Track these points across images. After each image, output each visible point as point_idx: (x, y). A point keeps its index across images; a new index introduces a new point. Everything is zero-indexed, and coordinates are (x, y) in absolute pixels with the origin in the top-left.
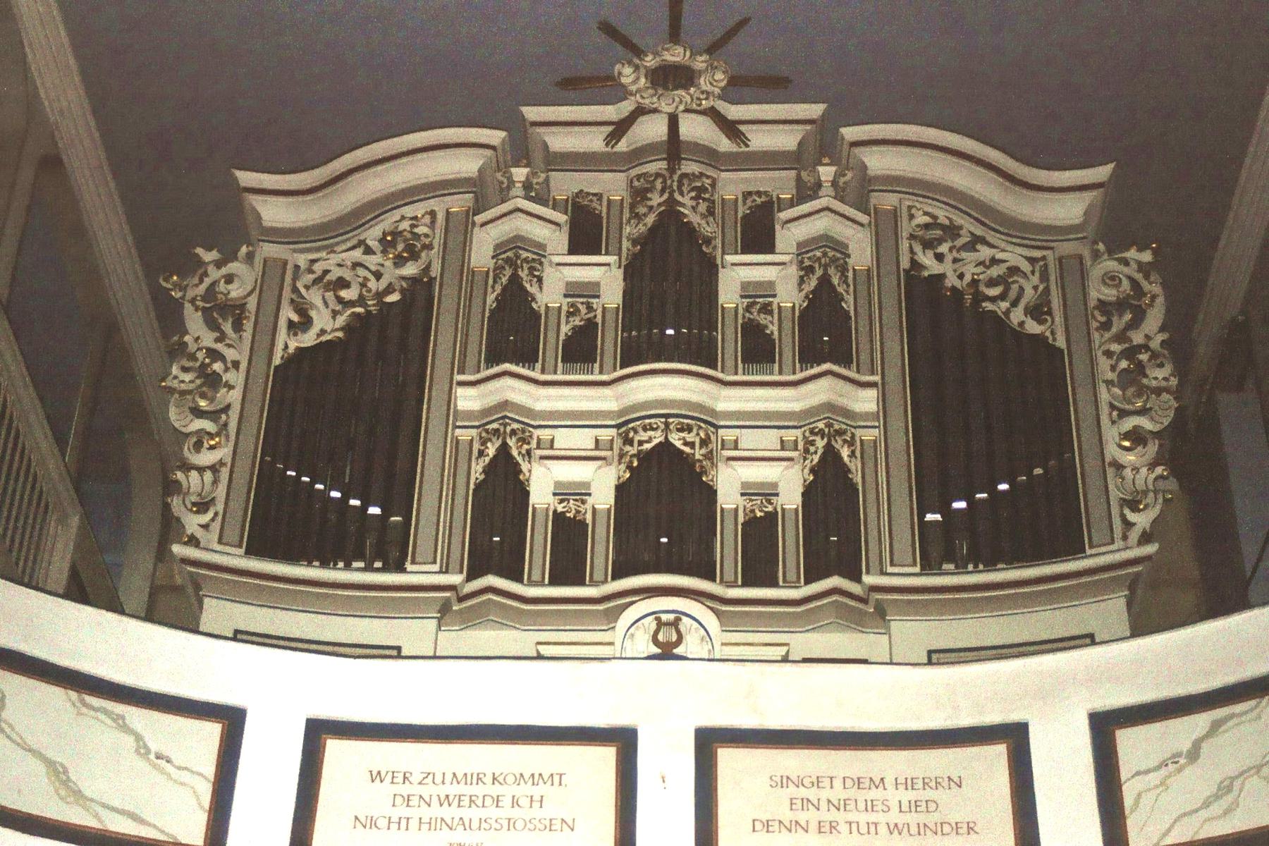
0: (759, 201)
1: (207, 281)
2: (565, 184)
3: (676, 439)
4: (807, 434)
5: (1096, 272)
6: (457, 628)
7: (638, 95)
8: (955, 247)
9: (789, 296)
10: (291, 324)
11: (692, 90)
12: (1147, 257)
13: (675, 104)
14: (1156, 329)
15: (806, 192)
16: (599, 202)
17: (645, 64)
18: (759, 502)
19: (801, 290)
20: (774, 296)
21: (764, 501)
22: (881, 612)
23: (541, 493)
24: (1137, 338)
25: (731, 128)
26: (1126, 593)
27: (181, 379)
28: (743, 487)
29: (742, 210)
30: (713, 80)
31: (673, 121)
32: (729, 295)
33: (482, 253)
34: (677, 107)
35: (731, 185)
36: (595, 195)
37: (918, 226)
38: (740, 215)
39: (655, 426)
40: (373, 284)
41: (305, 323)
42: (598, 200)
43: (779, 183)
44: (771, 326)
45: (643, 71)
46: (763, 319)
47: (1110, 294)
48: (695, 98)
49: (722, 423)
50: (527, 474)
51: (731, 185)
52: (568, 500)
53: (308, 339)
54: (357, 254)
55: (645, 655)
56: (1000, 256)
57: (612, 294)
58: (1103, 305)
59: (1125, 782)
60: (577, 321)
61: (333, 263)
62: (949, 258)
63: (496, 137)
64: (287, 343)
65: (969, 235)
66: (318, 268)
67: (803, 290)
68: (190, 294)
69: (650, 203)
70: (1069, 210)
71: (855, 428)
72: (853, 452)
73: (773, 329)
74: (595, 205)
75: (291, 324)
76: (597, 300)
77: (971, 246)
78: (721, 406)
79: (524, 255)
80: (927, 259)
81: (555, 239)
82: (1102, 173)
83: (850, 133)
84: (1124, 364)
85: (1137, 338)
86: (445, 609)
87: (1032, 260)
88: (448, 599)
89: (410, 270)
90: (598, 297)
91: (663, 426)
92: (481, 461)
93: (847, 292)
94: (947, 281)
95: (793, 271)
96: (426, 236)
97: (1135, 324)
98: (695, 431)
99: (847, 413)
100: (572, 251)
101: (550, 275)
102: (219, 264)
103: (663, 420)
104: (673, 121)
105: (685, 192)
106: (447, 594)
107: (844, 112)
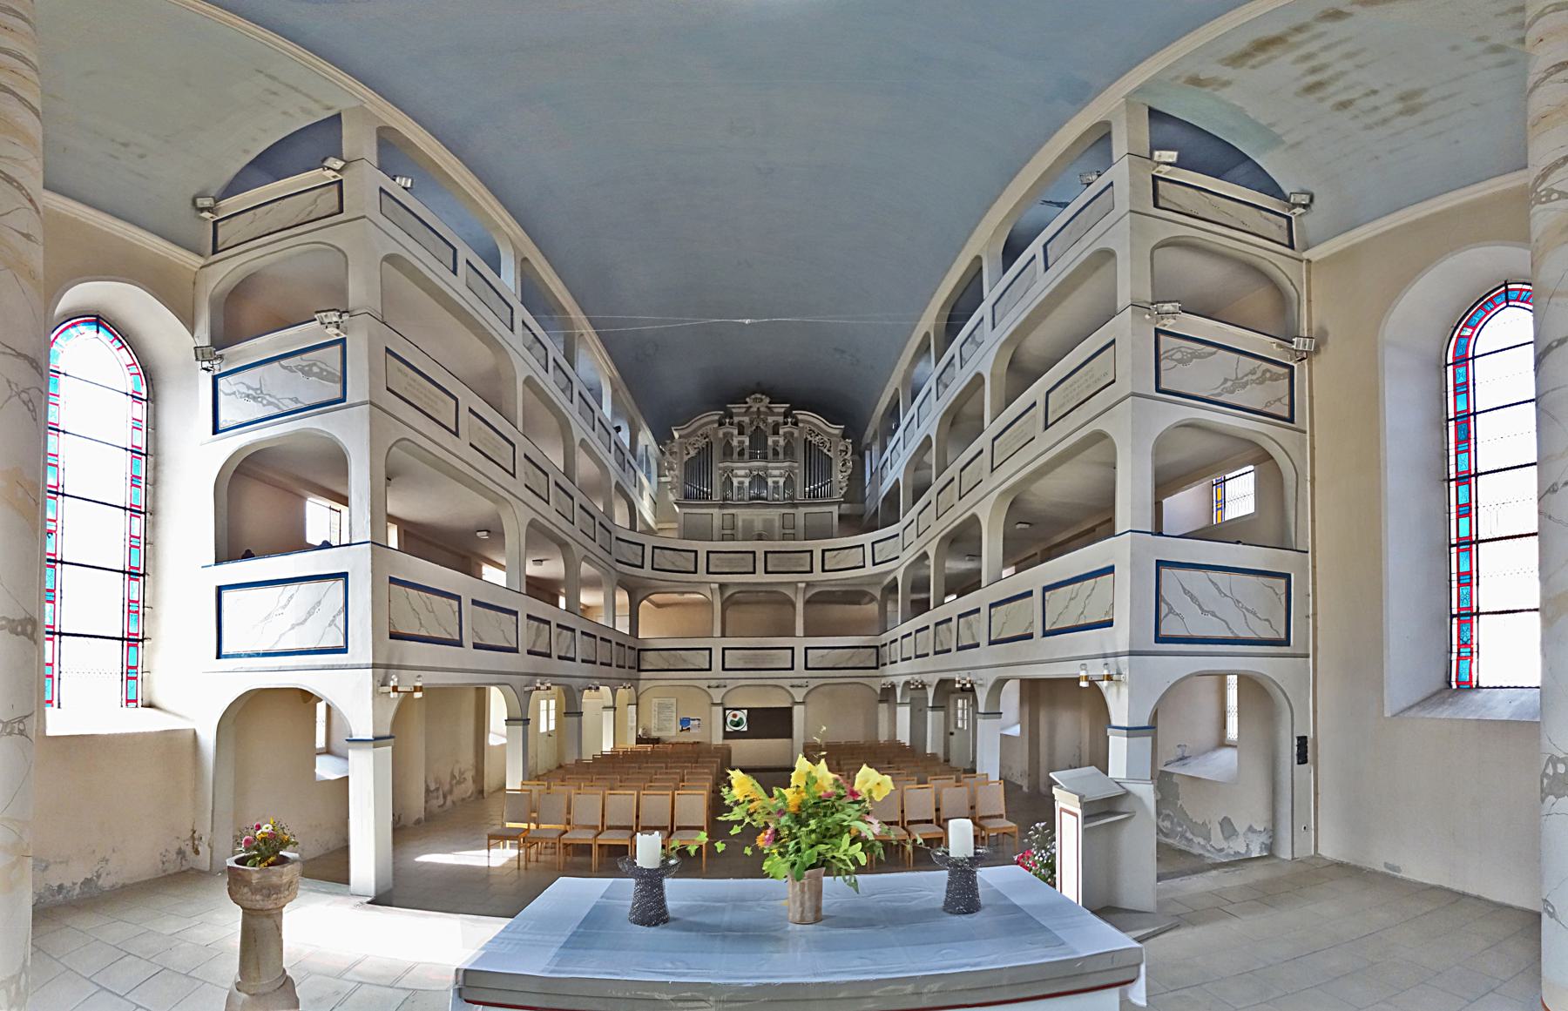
2: (736, 419)
9: (782, 442)
12: (850, 441)
14: (288, 868)
15: (786, 423)
23: (735, 481)
24: (846, 457)
25: (769, 408)
32: (770, 442)
33: (721, 435)
35: (770, 419)
41: (688, 454)
43: (781, 419)
47: (842, 448)
51: (770, 419)
52: (751, 499)
53: (689, 456)
55: (1176, 758)
58: (841, 450)
59: (1233, 632)
61: (692, 440)
64: (686, 458)
70: (836, 432)
80: (809, 437)
81: (736, 432)
82: (842, 427)
83: (794, 412)
85: (846, 457)
94: (756, 524)
101: (734, 439)
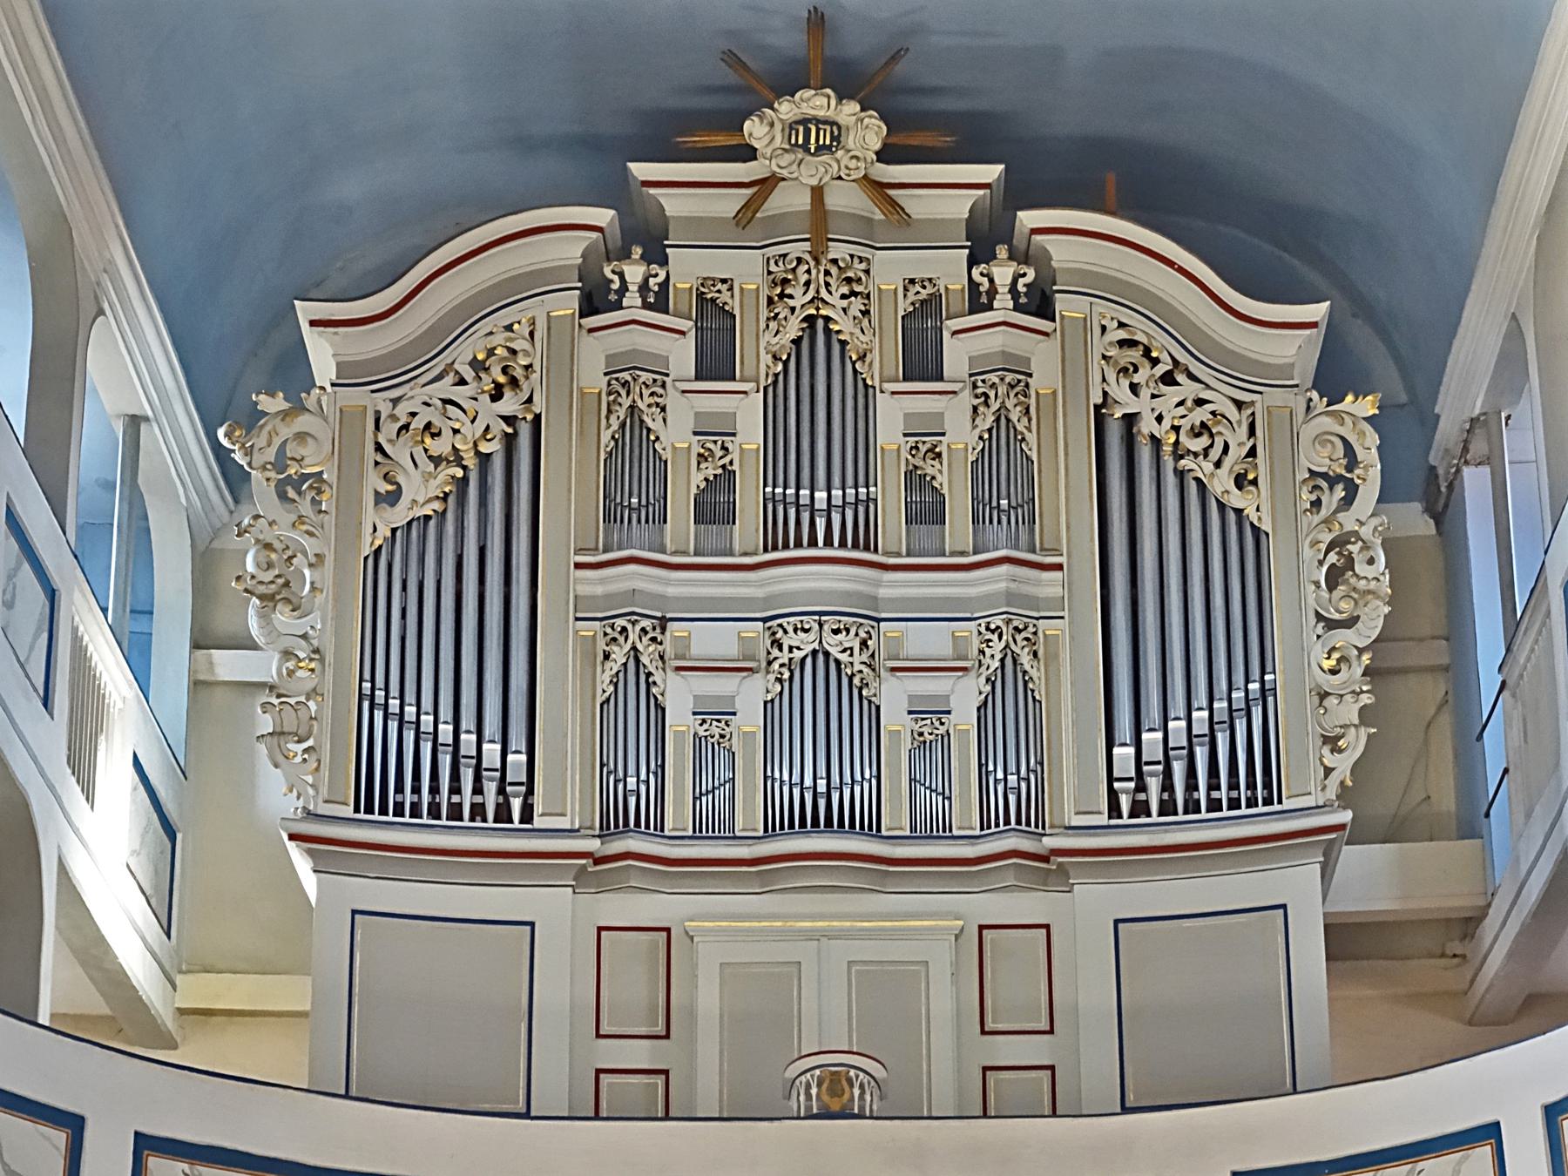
0: (924, 294)
1: (277, 442)
3: (833, 644)
4: (983, 629)
5: (1308, 432)
6: (593, 891)
7: (774, 161)
8: (1153, 375)
10: (379, 498)
11: (840, 153)
13: (818, 176)
16: (729, 293)
17: (781, 116)
18: (929, 721)
19: (975, 427)
20: (943, 434)
21: (934, 720)
22: (1062, 871)
26: (1322, 859)
27: (261, 579)
28: (910, 703)
29: (904, 306)
30: (868, 133)
31: (818, 193)
34: (821, 180)
36: (724, 281)
37: (1111, 344)
38: (901, 313)
39: (807, 626)
40: (467, 429)
42: (728, 290)
44: (938, 476)
45: (778, 126)
46: (930, 468)
48: (842, 167)
49: (884, 615)
50: (662, 686)
53: (400, 515)
54: (445, 388)
56: (1206, 395)
57: (751, 434)
60: (711, 470)
62: (1145, 393)
63: (603, 216)
65: (1170, 361)
66: (402, 411)
67: (977, 426)
68: (258, 459)
69: (791, 303)
71: (1037, 619)
72: (1035, 654)
73: (942, 481)
74: (725, 297)
75: (379, 498)
76: (732, 438)
77: (1168, 379)
78: (883, 592)
79: (645, 376)
80: (1120, 391)
83: (1028, 218)
84: (1333, 558)
85: (1348, 521)
86: (581, 873)
87: (1239, 405)
88: (584, 866)
89: (510, 404)
90: (734, 435)
91: (816, 627)
92: (608, 664)
93: (1029, 430)
95: (966, 399)
96: (525, 352)
97: (1348, 501)
98: (853, 632)
99: (1032, 602)
100: (699, 377)
102: (285, 415)
103: (817, 618)
104: (818, 193)
105: (833, 291)
106: (583, 862)
107: (1018, 193)
